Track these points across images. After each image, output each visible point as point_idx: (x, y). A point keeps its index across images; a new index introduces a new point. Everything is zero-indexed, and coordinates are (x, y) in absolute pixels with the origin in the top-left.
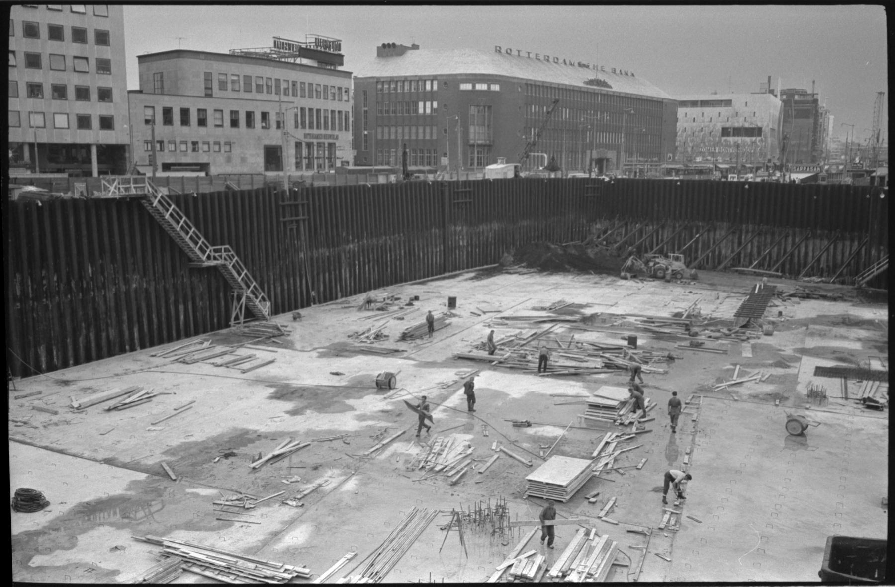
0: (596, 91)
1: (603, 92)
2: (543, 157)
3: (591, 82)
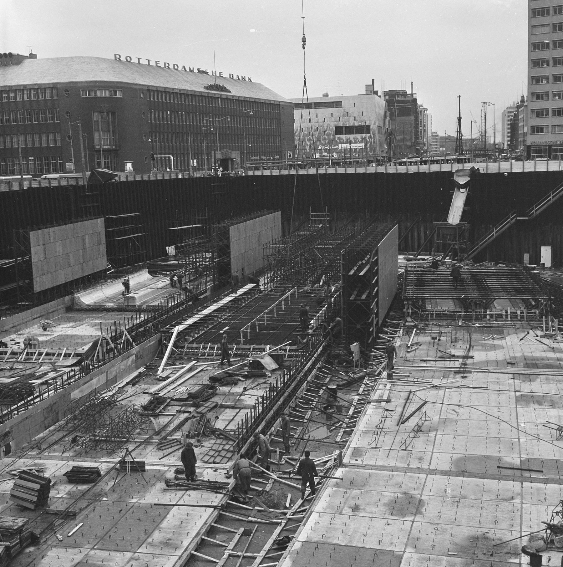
0: (216, 96)
1: (223, 97)
2: (169, 158)
3: (211, 87)
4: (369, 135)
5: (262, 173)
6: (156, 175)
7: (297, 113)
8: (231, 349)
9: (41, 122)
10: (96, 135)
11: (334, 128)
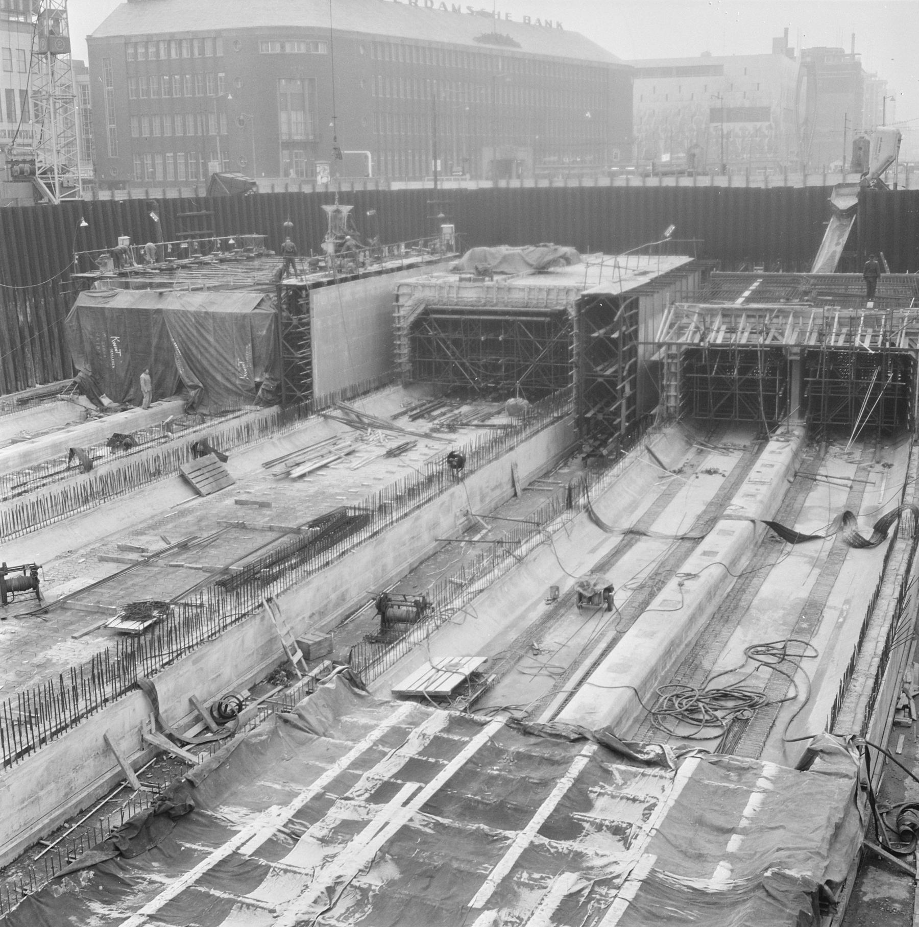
4: (767, 124)
5: (522, 184)
6: (339, 184)
7: (640, 86)
8: (268, 391)
9: (175, 96)
10: (283, 117)
11: (708, 111)
